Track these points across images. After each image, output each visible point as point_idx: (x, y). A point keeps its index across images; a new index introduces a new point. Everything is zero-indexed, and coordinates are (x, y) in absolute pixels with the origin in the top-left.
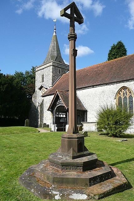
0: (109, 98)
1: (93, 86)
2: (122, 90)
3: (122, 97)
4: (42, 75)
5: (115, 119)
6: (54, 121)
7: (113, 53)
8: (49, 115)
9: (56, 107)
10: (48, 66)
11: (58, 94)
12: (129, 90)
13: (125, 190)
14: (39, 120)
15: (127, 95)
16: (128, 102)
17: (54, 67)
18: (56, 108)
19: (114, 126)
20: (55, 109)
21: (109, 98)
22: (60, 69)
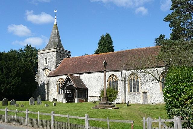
1: (92, 72)
3: (112, 81)
4: (45, 58)
5: (110, 94)
6: (64, 96)
7: (103, 43)
8: (55, 92)
9: (66, 86)
10: (52, 51)
11: (69, 77)
12: (116, 77)
13: (140, 7)
14: (46, 96)
15: (114, 79)
16: (115, 83)
17: (57, 53)
18: (66, 87)
19: (110, 97)
20: (65, 88)
22: (62, 54)
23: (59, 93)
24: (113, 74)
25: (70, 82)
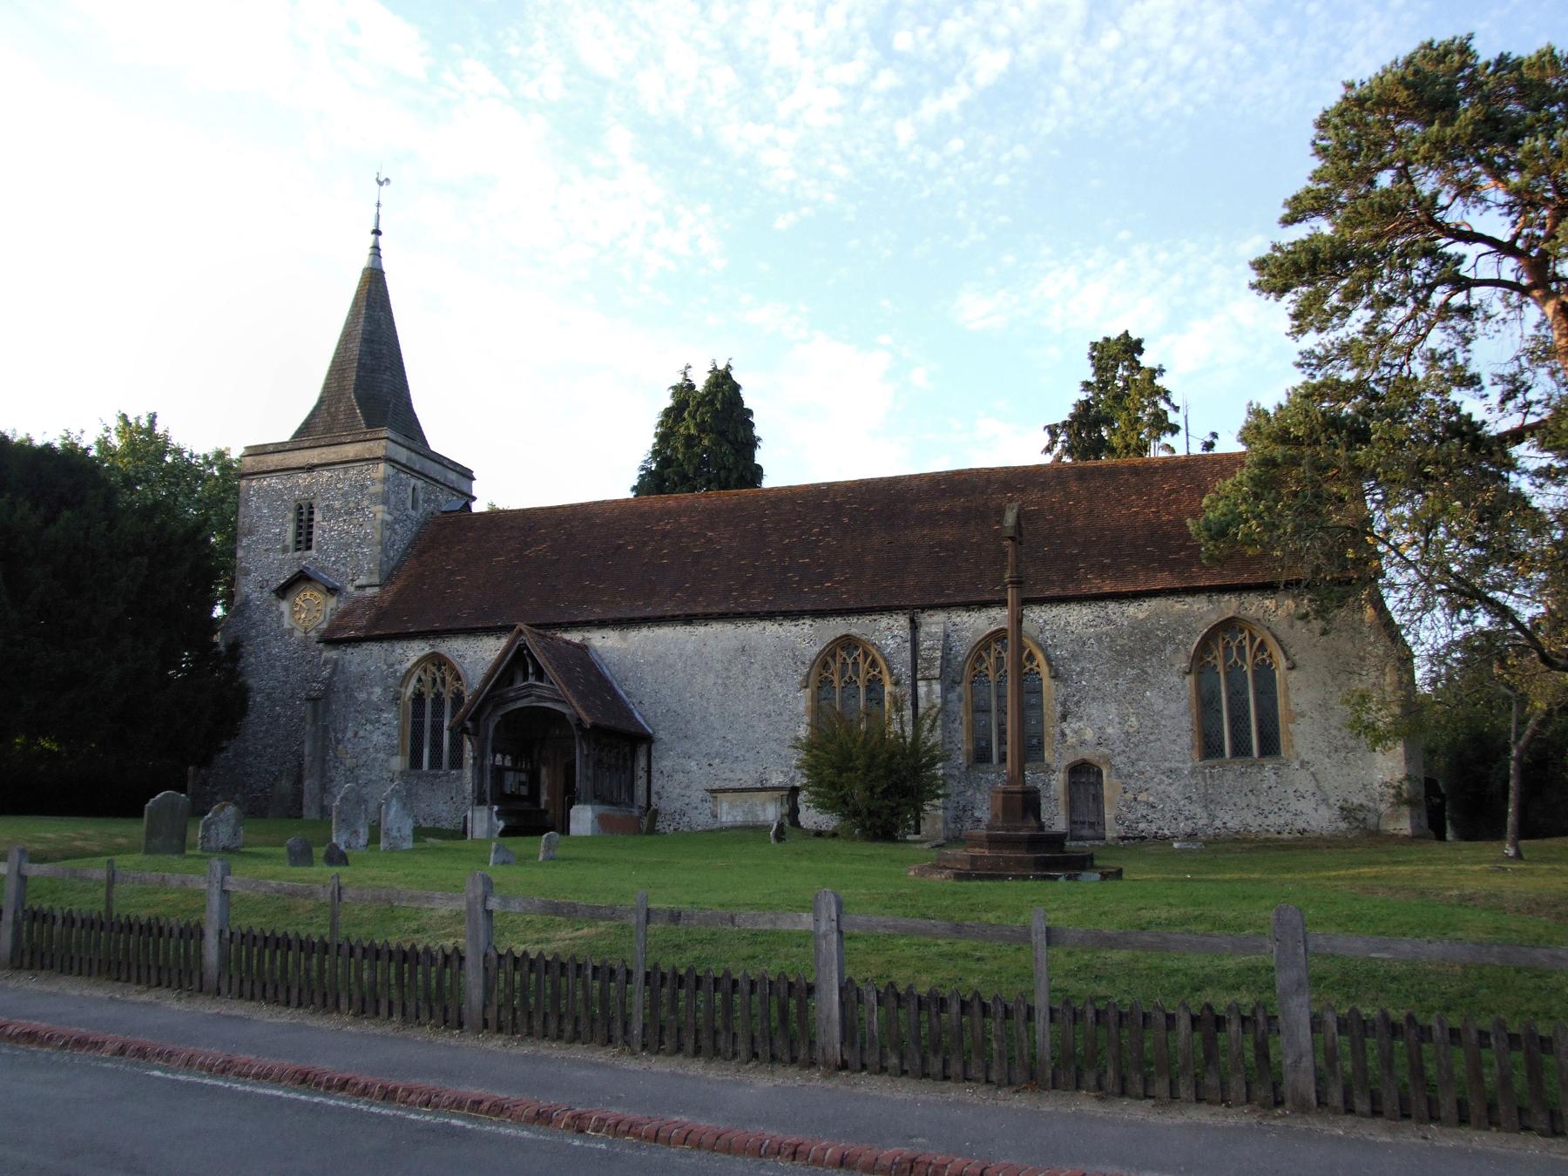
0: (775, 683)
2: (838, 650)
4: (293, 505)
8: (382, 755)
12: (866, 655)
21: (775, 683)
22: (420, 484)
23: (416, 761)
24: (854, 631)
25: (532, 680)
